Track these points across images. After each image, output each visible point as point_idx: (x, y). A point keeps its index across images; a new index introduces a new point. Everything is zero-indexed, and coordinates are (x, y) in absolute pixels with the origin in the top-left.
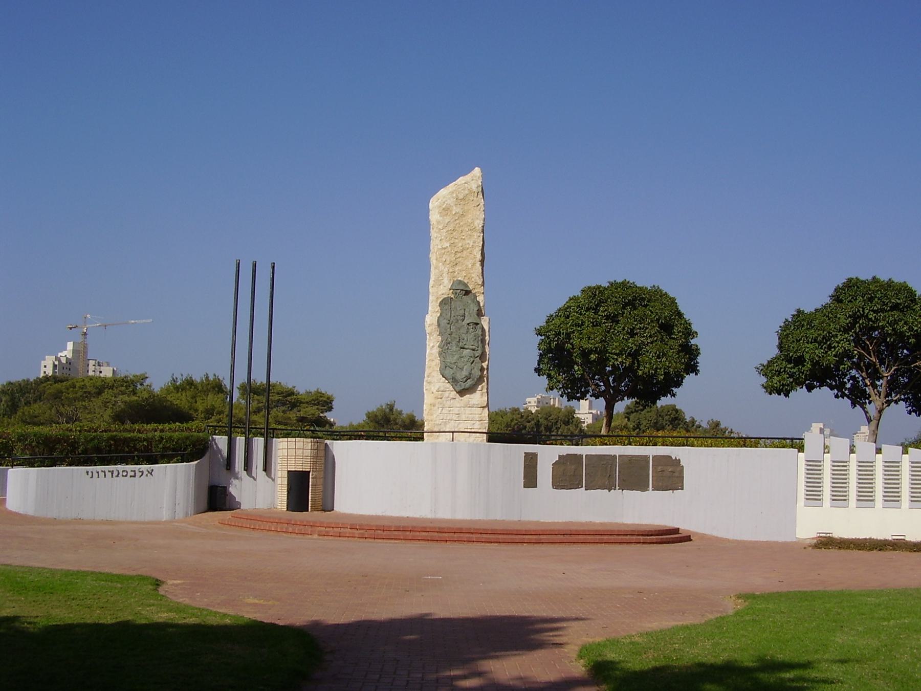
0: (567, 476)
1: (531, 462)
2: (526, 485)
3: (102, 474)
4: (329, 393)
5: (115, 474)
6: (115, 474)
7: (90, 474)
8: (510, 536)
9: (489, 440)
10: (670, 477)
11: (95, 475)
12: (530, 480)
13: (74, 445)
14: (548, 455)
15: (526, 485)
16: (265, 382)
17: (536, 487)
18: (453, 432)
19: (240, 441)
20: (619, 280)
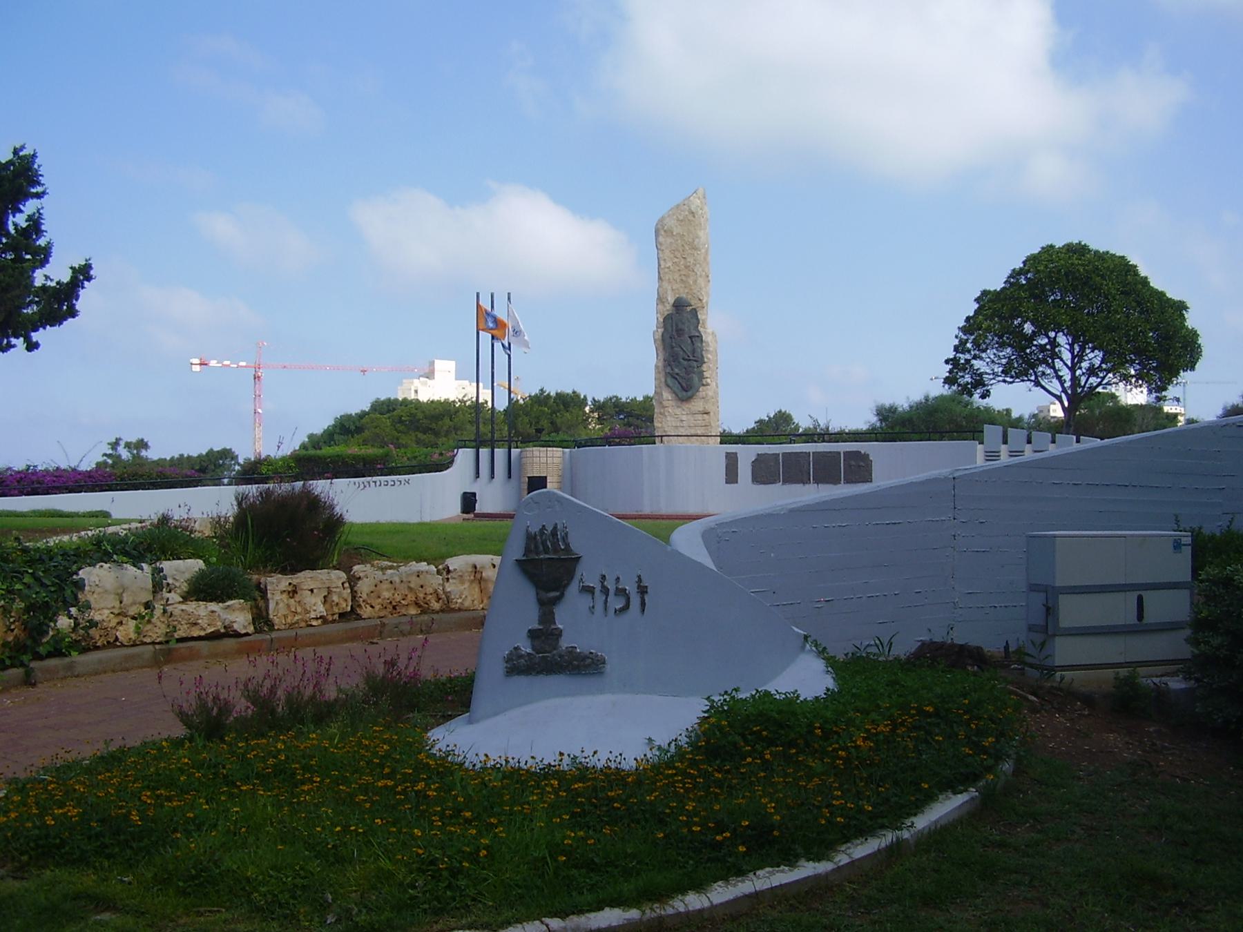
0: (764, 472)
9: (721, 443)
12: (731, 475)
14: (747, 454)
19: (485, 452)
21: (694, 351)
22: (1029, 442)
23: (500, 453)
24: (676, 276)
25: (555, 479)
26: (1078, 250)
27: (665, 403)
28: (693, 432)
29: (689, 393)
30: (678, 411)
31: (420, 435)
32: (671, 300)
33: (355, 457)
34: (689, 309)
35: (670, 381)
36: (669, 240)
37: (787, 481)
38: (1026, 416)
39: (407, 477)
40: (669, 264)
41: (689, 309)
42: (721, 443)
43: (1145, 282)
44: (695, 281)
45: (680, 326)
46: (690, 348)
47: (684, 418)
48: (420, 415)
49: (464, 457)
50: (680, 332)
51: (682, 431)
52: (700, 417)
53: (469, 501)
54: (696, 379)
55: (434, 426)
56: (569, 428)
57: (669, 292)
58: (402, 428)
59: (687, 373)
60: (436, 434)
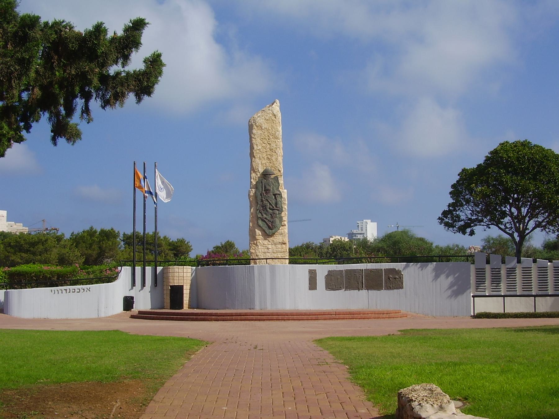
0: (333, 282)
1: (313, 276)
2: (310, 289)
3: (60, 292)
4: (87, 228)
5: (68, 291)
6: (68, 291)
7: (53, 291)
8: (301, 316)
9: (290, 263)
10: (394, 281)
11: (56, 292)
12: (313, 285)
13: (45, 277)
14: (322, 270)
15: (310, 289)
16: (142, 234)
17: (310, 289)
18: (267, 259)
19: (138, 269)
20: (455, 179)
21: (276, 204)
22: (488, 262)
23: (149, 269)
24: (264, 155)
25: (188, 287)
26: (525, 144)
27: (257, 237)
28: (275, 256)
29: (273, 231)
30: (266, 242)
31: (23, 255)
32: (261, 170)
33: (52, 273)
34: (272, 176)
35: (260, 222)
36: (260, 132)
37: (347, 288)
38: (434, 245)
39: (88, 286)
40: (260, 147)
41: (272, 176)
42: (290, 263)
43: (479, 166)
44: (277, 159)
45: (268, 187)
46: (274, 202)
47: (270, 247)
48: (22, 242)
49: (125, 272)
50: (267, 191)
51: (269, 255)
52: (279, 246)
53: (128, 303)
54: (277, 221)
55: (32, 249)
56: (110, 250)
57: (260, 166)
58: (12, 250)
59: (272, 217)
60: (34, 254)
